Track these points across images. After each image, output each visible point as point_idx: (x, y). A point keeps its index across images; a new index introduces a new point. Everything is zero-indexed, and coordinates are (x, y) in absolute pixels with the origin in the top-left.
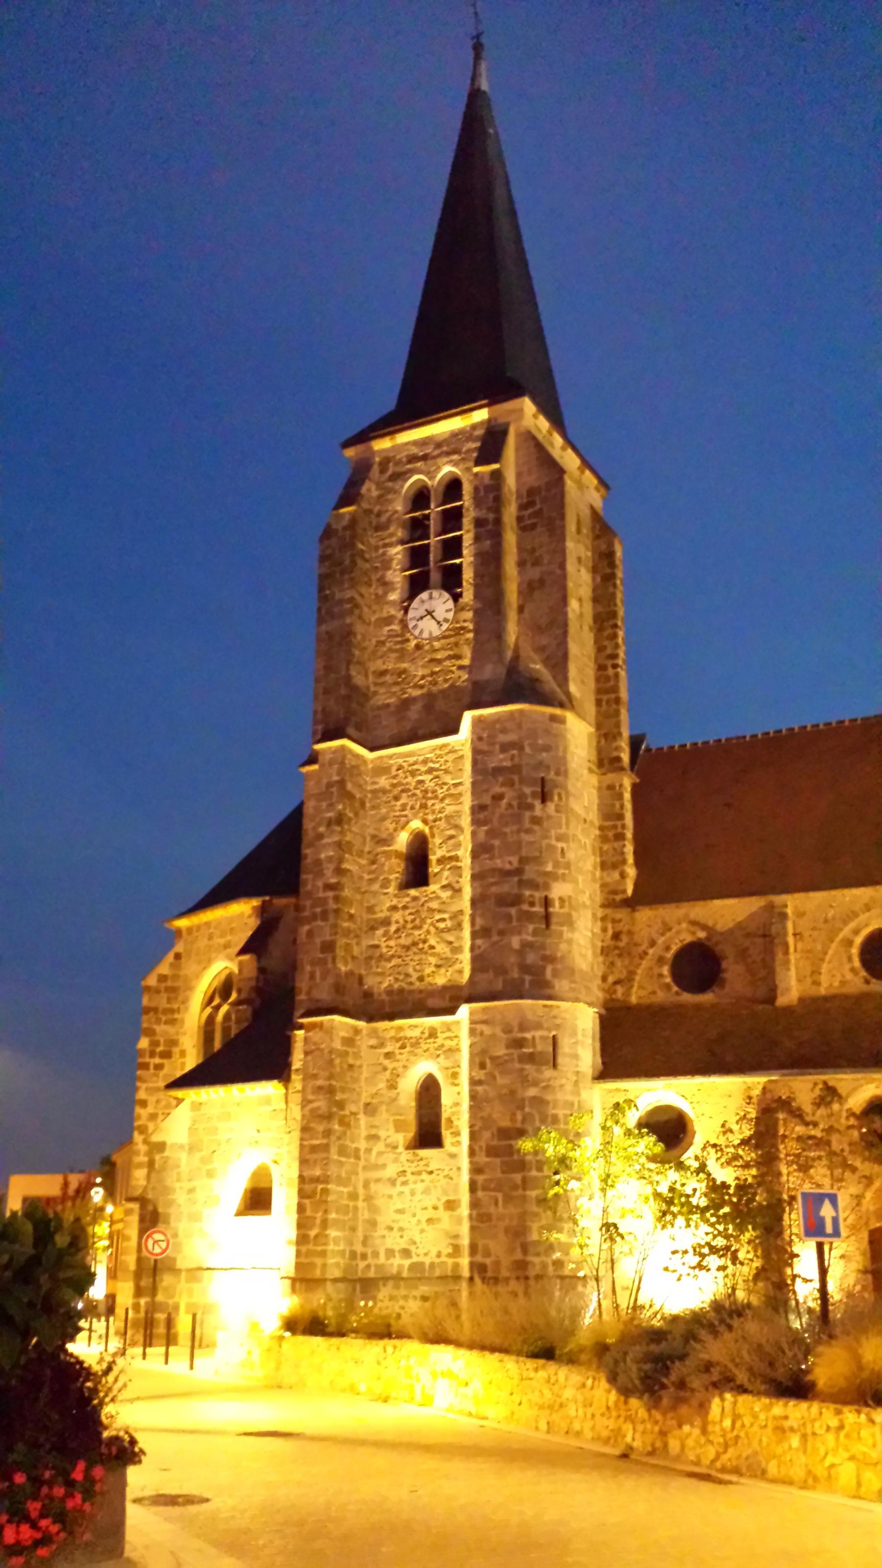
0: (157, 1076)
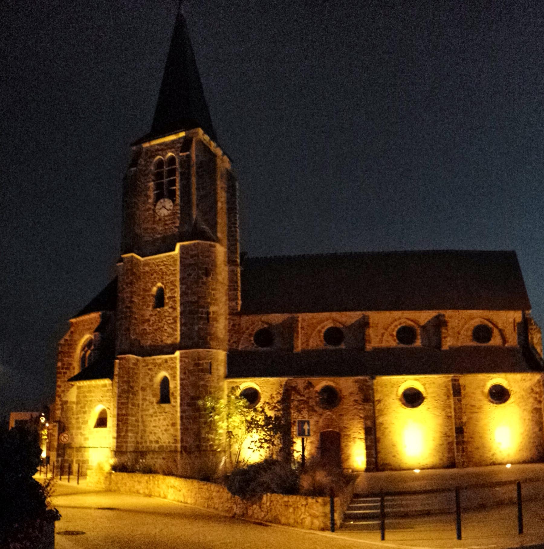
0: (64, 376)
